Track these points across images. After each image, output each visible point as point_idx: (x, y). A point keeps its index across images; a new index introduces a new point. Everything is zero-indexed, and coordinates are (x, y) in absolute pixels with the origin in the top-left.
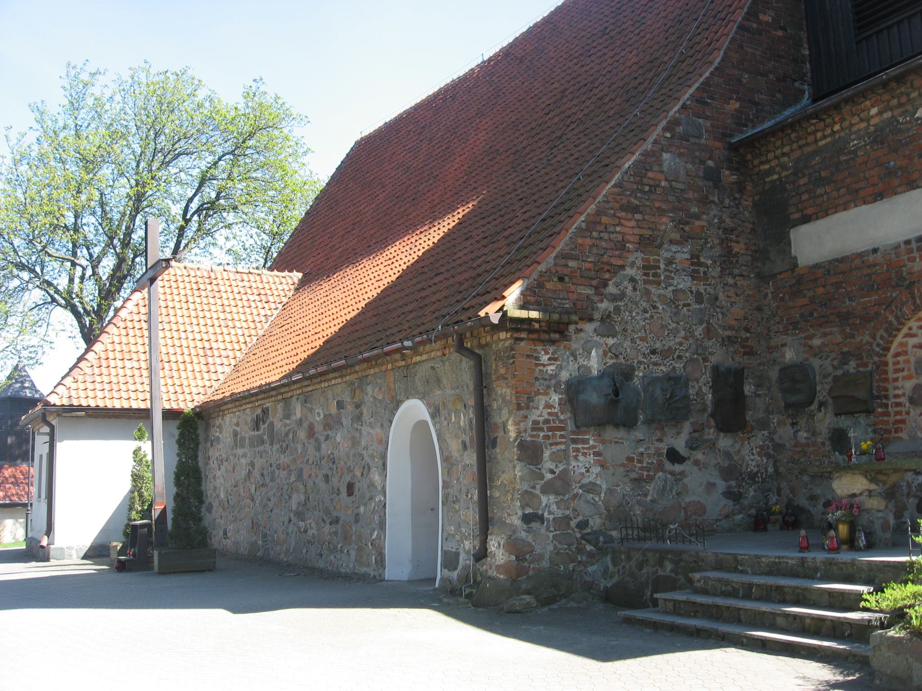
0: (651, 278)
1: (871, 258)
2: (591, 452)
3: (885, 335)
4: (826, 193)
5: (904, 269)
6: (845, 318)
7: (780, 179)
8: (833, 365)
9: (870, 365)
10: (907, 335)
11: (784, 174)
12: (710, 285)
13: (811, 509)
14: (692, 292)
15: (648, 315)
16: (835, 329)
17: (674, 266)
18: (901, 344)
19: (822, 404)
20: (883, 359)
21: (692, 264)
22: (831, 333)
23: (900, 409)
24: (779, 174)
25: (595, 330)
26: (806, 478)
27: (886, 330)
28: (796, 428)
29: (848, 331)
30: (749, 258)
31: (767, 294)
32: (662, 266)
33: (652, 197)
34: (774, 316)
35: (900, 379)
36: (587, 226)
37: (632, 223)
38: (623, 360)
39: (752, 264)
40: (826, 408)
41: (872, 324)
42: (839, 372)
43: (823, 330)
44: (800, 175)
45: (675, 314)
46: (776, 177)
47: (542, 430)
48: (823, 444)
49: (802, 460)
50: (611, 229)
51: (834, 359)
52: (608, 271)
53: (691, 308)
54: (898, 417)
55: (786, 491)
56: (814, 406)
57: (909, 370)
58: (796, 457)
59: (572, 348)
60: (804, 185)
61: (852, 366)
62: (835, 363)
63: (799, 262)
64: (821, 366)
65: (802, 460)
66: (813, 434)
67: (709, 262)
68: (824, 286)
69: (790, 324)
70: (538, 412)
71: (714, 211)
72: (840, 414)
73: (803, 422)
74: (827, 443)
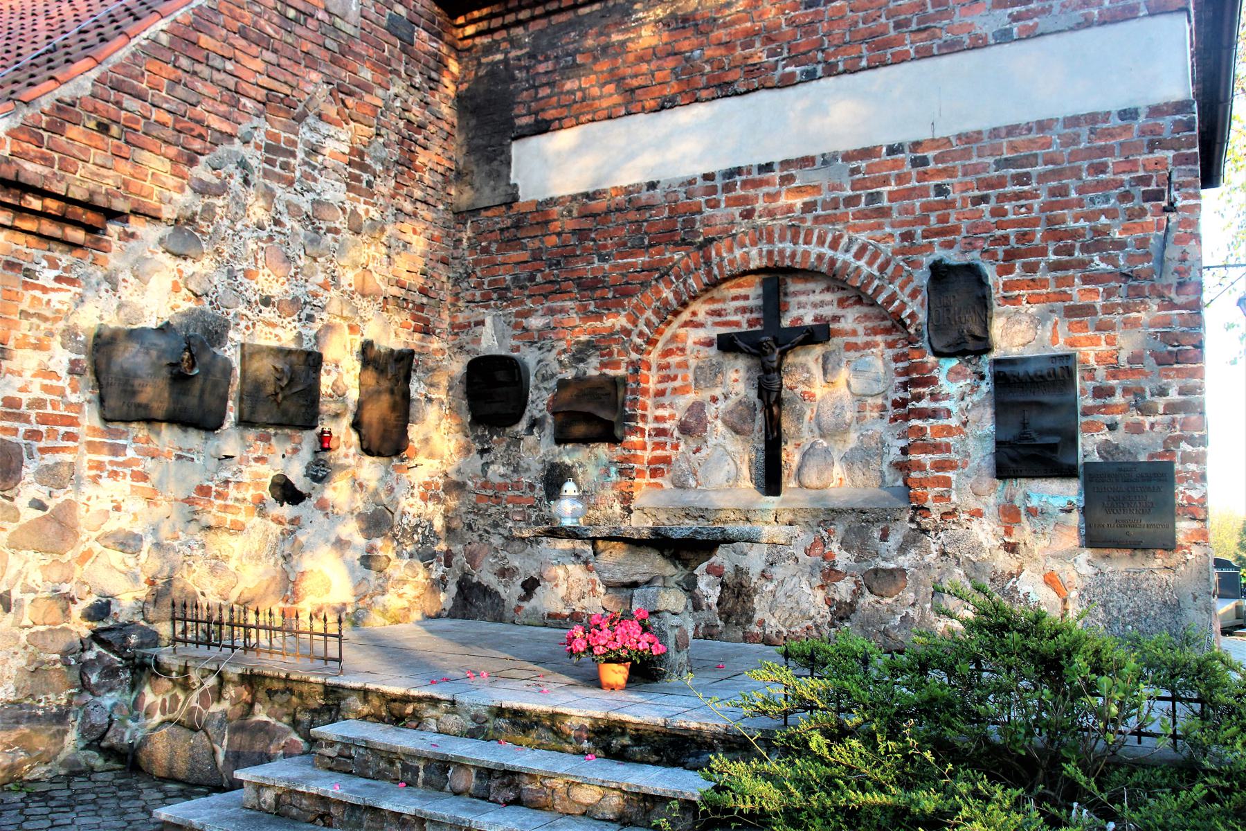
0: (277, 169)
1: (644, 196)
2: (128, 471)
3: (654, 320)
4: (580, 89)
5: (698, 217)
6: (588, 286)
7: (506, 61)
8: (560, 362)
9: (623, 365)
10: (686, 324)
11: (514, 53)
12: (374, 205)
13: (501, 589)
14: (344, 210)
15: (264, 234)
16: (569, 304)
17: (320, 158)
18: (674, 338)
19: (534, 423)
20: (645, 357)
21: (350, 164)
22: (562, 310)
23: (662, 439)
24: (507, 53)
25: (161, 241)
26: (496, 541)
27: (657, 312)
28: (487, 458)
29: (592, 308)
30: (440, 178)
31: (460, 240)
32: (301, 155)
33: (298, 30)
34: (469, 276)
35: (668, 392)
36: (171, 42)
37: (258, 65)
38: (208, 307)
39: (444, 189)
40: (542, 429)
41: (634, 301)
42: (569, 374)
43: (547, 304)
44: (540, 58)
45: (312, 241)
46: (499, 57)
47: (26, 419)
48: (531, 487)
49: (493, 510)
50: (218, 62)
51: (565, 351)
52: (201, 136)
53: (339, 237)
54: (659, 453)
55: (460, 559)
56: (522, 426)
57: (685, 379)
58: (482, 505)
59: (110, 267)
60: (547, 73)
61: (592, 368)
62: (563, 357)
63: (520, 193)
64: (539, 362)
65: (493, 510)
66: (515, 471)
67: (379, 168)
68: (559, 234)
69: (495, 290)
70: (18, 382)
71: (398, 87)
72: (566, 442)
73: (499, 450)
74: (539, 486)
